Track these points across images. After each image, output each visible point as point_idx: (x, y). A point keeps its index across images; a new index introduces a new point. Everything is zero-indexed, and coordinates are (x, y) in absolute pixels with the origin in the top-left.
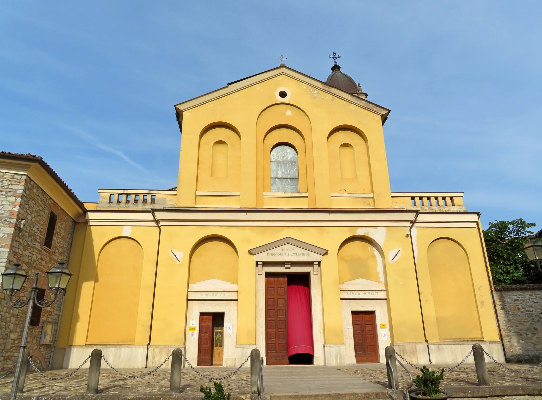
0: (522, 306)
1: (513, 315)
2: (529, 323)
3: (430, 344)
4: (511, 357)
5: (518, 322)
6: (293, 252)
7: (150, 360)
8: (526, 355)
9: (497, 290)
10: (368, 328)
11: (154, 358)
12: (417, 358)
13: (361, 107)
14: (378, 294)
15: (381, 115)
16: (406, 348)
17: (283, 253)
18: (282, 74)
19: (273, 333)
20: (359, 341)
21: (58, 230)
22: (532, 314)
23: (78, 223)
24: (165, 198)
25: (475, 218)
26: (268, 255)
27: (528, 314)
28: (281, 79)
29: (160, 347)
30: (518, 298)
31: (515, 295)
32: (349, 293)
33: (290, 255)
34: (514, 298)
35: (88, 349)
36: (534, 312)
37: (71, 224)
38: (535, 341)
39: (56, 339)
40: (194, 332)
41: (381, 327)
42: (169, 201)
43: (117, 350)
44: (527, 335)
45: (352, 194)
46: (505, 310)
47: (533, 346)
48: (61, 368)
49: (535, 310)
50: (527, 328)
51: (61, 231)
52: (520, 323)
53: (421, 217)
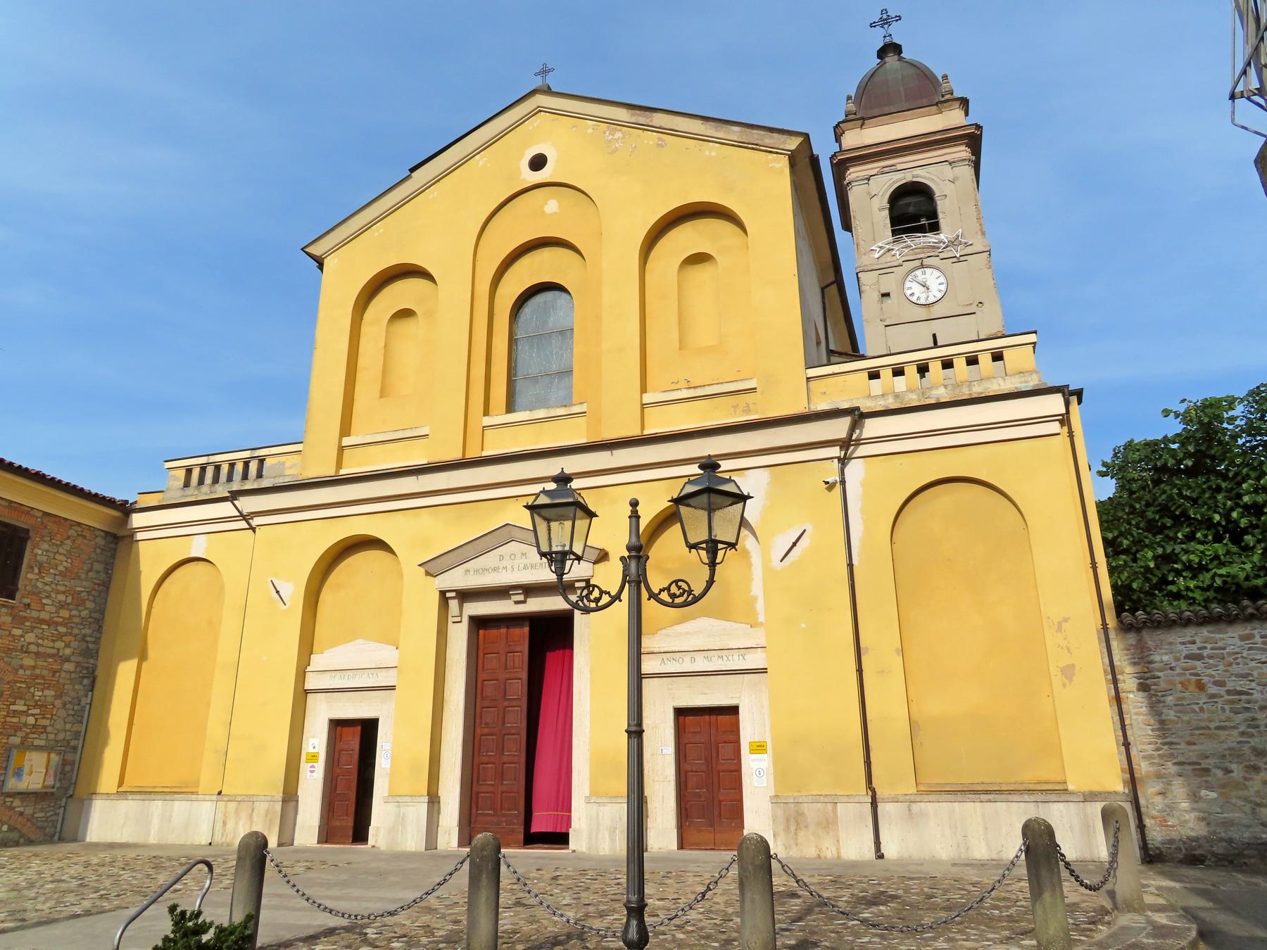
0: (1212, 676)
1: (1180, 706)
2: (1235, 733)
3: (883, 799)
4: (1163, 844)
5: (1198, 729)
6: (524, 561)
7: (218, 828)
8: (1221, 840)
9: (1125, 628)
10: (725, 750)
11: (225, 823)
12: (838, 841)
13: (733, 145)
14: (745, 657)
15: (786, 154)
16: (806, 811)
18: (538, 110)
19: (491, 766)
20: (697, 789)
22: (1249, 702)
24: (283, 463)
25: (1055, 404)
26: (466, 574)
27: (1232, 702)
28: (535, 124)
29: (237, 799)
30: (1199, 649)
31: (1190, 639)
32: (665, 660)
33: (516, 569)
34: (1185, 650)
36: (1256, 696)
38: (1258, 791)
40: (315, 764)
41: (752, 751)
42: (290, 468)
43: (167, 804)
44: (1228, 771)
45: (699, 389)
46: (1152, 692)
47: (1248, 808)
48: (75, 840)
49: (1259, 688)
50: (1230, 749)
52: (1203, 731)
53: (872, 427)
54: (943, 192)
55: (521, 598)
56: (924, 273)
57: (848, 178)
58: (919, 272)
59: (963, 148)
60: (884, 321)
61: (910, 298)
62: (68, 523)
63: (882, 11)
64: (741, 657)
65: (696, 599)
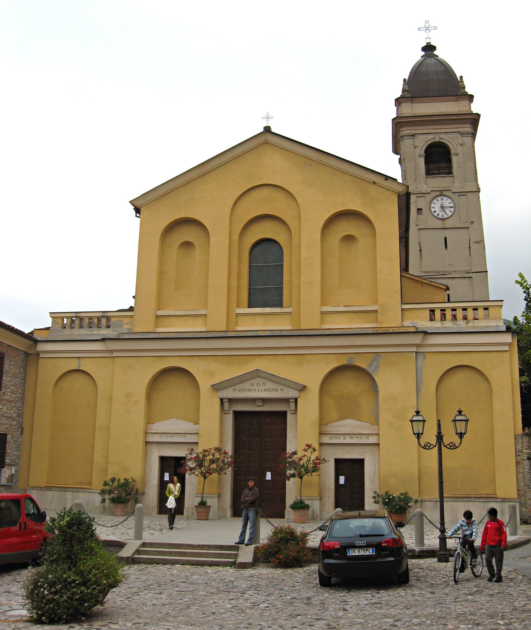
6: (264, 387)
17: (253, 388)
21: (7, 369)
23: (31, 354)
24: (122, 321)
26: (234, 391)
33: (260, 391)
35: (47, 491)
37: (22, 357)
39: (18, 480)
51: (10, 368)
54: (456, 151)
55: (261, 404)
56: (442, 199)
57: (402, 133)
58: (439, 198)
59: (469, 125)
60: (418, 226)
61: (434, 213)
62: (14, 349)
63: (426, 21)
64: (367, 438)
65: (457, 447)
